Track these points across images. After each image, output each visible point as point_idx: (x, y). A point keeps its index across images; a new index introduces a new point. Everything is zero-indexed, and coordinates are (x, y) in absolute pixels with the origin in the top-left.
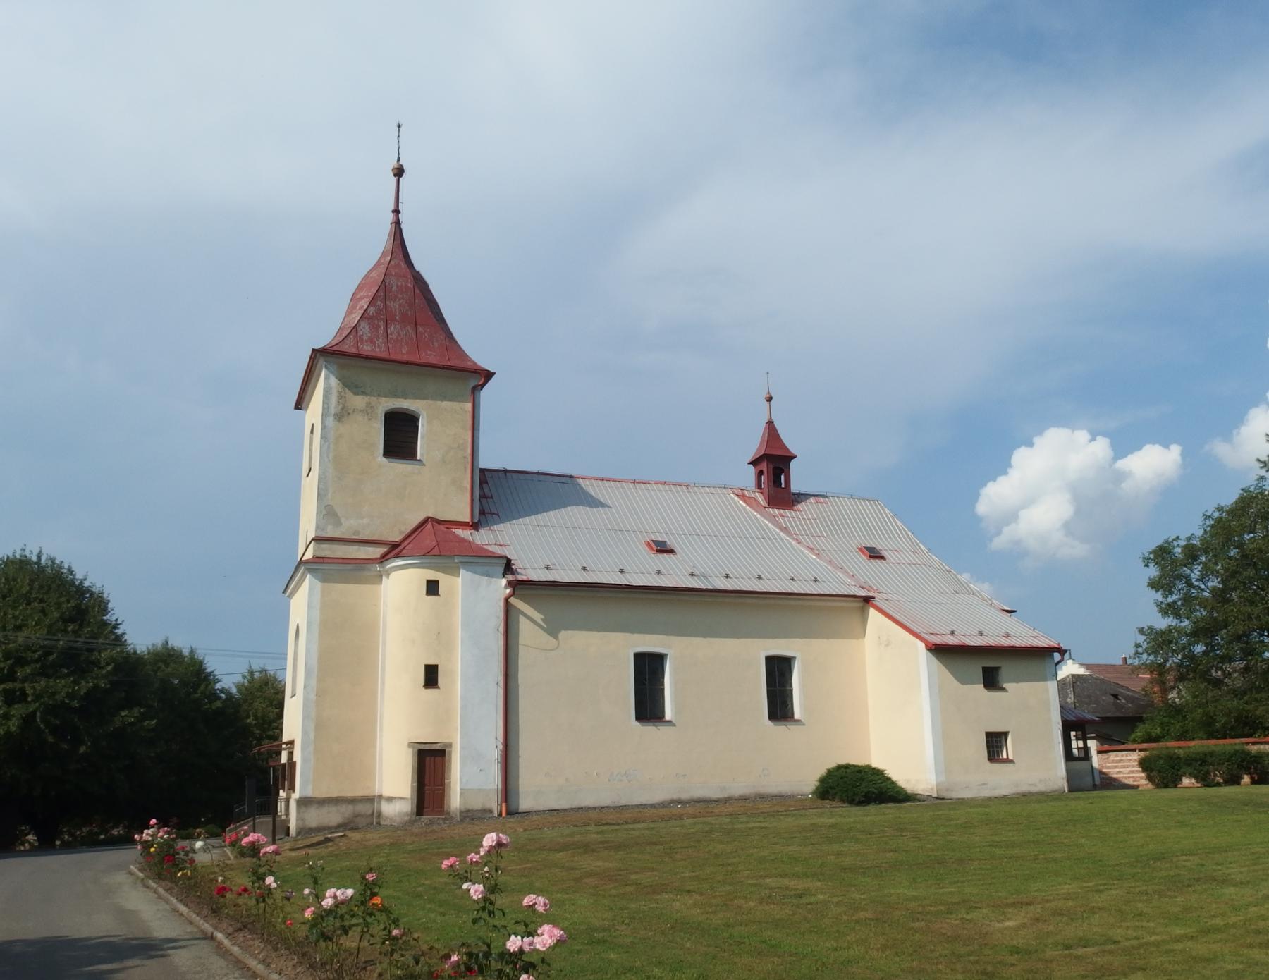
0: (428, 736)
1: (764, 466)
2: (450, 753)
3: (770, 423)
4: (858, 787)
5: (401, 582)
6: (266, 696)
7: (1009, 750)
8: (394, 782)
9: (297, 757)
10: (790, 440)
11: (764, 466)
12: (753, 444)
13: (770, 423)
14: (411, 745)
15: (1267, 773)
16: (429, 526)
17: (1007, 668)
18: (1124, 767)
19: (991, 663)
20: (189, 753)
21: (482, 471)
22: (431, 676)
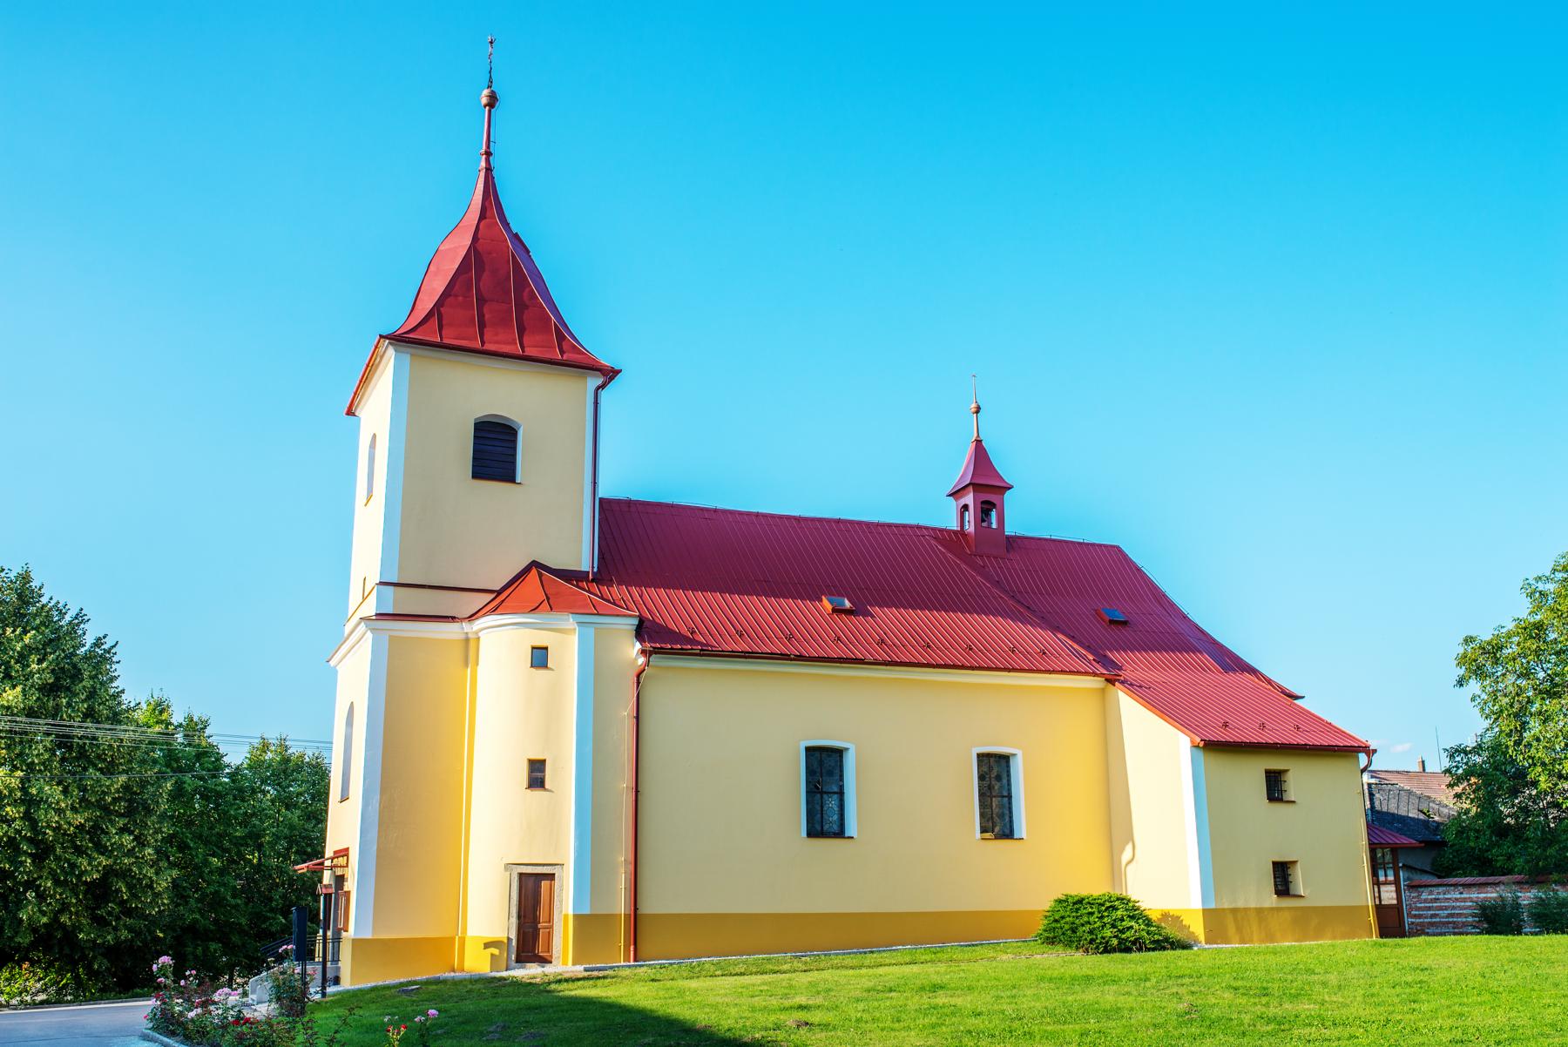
0: (534, 856)
1: (969, 499)
2: (561, 879)
3: (979, 442)
4: (1104, 927)
5: (502, 641)
6: (300, 786)
7: (1300, 882)
8: (486, 918)
9: (351, 885)
10: (1005, 466)
11: (969, 499)
12: (959, 468)
13: (979, 442)
14: (508, 866)
15: (1551, 920)
16: (534, 571)
17: (330, 975)
18: (1441, 908)
19: (1276, 763)
20: (217, 871)
21: (604, 503)
22: (537, 775)
